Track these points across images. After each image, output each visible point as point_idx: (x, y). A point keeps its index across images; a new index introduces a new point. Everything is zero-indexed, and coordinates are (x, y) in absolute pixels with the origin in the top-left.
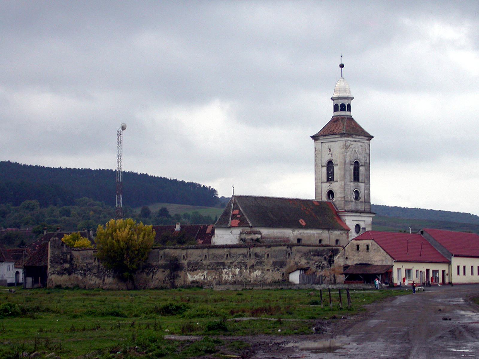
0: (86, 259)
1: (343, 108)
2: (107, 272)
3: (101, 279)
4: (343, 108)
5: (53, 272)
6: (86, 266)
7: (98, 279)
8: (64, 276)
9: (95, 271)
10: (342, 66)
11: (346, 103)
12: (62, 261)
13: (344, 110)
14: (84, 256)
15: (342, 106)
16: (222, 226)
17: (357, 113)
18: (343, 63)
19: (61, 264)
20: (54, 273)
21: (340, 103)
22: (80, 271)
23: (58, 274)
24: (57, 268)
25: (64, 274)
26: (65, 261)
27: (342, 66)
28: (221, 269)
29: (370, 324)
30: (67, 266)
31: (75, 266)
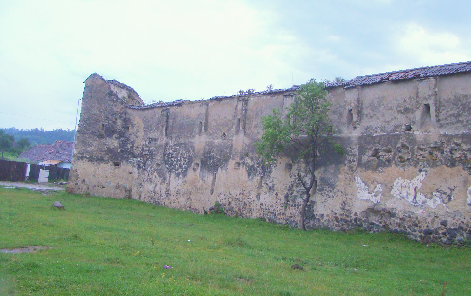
5: (82, 154)
8: (102, 165)
20: (82, 158)
23: (91, 160)
24: (90, 145)
26: (110, 132)
30: (113, 142)
31: (129, 146)
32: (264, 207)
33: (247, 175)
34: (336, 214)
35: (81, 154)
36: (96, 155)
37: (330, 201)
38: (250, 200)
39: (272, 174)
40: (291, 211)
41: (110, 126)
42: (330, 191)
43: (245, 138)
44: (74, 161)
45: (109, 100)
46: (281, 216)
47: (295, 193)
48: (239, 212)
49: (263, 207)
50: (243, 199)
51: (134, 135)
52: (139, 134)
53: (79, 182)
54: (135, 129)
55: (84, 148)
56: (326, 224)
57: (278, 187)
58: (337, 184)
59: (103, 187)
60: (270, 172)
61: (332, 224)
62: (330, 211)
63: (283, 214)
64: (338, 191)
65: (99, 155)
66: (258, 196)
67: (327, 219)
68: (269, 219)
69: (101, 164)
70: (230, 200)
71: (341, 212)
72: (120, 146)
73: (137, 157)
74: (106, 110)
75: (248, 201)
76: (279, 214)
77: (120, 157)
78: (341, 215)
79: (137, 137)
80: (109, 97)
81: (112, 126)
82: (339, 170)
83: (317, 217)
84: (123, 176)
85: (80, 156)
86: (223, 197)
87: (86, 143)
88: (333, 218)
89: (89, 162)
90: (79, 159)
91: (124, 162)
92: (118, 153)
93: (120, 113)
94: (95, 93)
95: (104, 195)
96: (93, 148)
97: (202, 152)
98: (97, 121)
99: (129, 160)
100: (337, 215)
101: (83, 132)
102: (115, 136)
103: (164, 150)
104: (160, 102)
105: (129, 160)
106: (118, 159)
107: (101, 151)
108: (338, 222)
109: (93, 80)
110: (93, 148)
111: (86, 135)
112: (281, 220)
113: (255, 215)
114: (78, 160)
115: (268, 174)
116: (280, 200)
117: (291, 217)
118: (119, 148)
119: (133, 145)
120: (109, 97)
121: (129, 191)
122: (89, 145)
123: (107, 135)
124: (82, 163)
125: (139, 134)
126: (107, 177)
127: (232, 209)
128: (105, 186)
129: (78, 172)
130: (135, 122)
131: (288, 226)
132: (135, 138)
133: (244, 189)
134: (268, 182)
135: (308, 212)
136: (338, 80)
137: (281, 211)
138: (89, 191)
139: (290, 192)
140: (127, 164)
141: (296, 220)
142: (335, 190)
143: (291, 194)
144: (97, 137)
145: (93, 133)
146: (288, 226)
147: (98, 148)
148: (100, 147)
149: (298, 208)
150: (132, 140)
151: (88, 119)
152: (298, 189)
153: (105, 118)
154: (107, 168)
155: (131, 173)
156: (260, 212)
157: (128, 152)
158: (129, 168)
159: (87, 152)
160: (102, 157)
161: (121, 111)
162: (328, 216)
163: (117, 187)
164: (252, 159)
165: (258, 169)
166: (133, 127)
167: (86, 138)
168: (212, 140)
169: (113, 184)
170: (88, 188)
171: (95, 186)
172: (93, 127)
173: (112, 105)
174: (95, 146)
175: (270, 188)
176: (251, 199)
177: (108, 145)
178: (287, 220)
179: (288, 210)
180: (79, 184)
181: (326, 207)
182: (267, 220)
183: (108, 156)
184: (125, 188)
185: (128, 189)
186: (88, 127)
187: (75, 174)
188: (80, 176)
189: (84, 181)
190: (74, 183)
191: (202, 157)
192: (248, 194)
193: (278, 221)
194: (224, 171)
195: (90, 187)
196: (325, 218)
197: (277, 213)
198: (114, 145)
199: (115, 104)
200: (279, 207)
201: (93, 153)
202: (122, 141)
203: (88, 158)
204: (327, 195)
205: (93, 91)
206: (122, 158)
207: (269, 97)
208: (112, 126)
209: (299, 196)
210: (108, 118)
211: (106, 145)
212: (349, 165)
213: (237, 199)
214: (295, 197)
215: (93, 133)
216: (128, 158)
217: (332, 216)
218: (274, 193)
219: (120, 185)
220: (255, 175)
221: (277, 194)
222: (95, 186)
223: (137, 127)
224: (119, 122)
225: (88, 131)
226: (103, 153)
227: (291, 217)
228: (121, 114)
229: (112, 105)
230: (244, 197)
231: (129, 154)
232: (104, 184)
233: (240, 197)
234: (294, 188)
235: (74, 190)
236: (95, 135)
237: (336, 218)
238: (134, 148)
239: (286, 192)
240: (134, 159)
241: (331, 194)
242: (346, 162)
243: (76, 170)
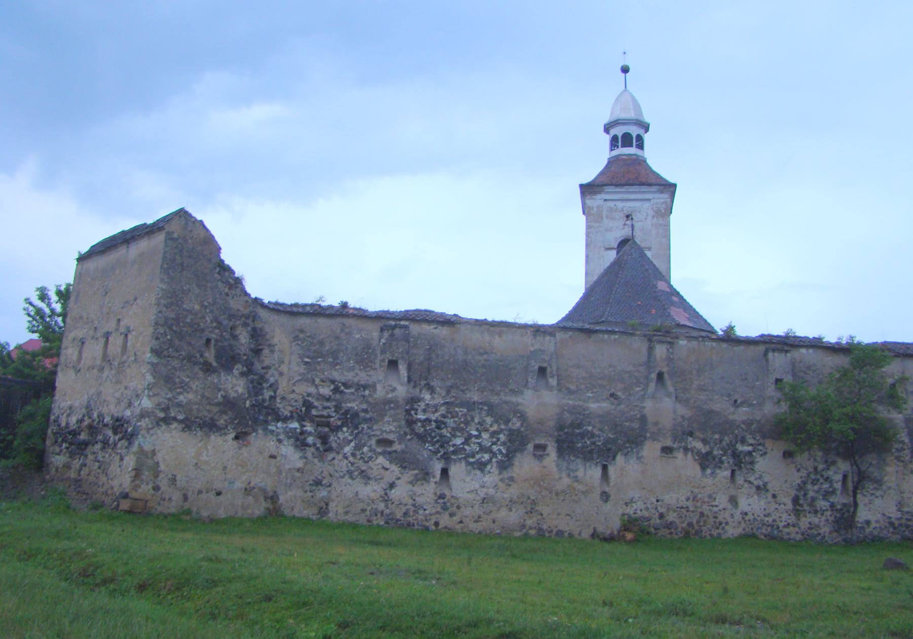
0: (334, 365)
1: (627, 140)
2: (467, 442)
3: (426, 475)
4: (627, 140)
5: (166, 409)
8: (215, 439)
9: (389, 427)
10: (625, 70)
11: (634, 131)
12: (210, 355)
13: (631, 146)
14: (322, 343)
15: (627, 135)
16: (528, 339)
17: (658, 157)
18: (627, 64)
19: (208, 368)
20: (167, 421)
21: (619, 131)
23: (188, 425)
24: (185, 387)
27: (625, 70)
28: (494, 455)
29: (137, 512)
30: (235, 385)
31: (267, 394)
33: (698, 468)
34: (890, 518)
35: (163, 410)
36: (200, 415)
37: (878, 502)
38: (715, 509)
39: (757, 467)
42: (874, 488)
43: (678, 406)
44: (148, 430)
45: (220, 280)
46: (791, 528)
47: (811, 494)
49: (750, 517)
50: (696, 507)
51: (276, 369)
53: (163, 483)
55: (170, 395)
56: (875, 533)
57: (774, 486)
59: (219, 494)
60: (752, 463)
61: (885, 532)
62: (879, 516)
63: (794, 526)
64: (889, 488)
65: (206, 414)
66: (733, 500)
67: (878, 525)
68: (765, 536)
69: (213, 437)
70: (661, 510)
71: (899, 515)
73: (285, 419)
74: (215, 303)
76: (785, 526)
78: (898, 519)
79: (281, 374)
80: (219, 273)
82: (884, 460)
84: (258, 464)
85: (162, 415)
86: (643, 506)
87: (175, 383)
89: (183, 430)
90: (159, 422)
91: (260, 431)
92: (247, 409)
93: (243, 315)
94: (190, 257)
96: (191, 396)
97: (552, 423)
98: (196, 330)
99: (270, 427)
100: (893, 520)
101: (165, 353)
102: (238, 368)
103: (408, 412)
104: (344, 305)
106: (247, 425)
107: (209, 404)
108: (895, 528)
109: (186, 224)
111: (175, 363)
112: (792, 536)
114: (158, 425)
115: (748, 466)
116: (785, 505)
117: (811, 528)
119: (275, 392)
120: (219, 273)
121: (272, 498)
122: (182, 387)
123: (223, 366)
124: (167, 435)
125: (284, 368)
126: (225, 468)
127: (669, 525)
129: (159, 457)
130: (275, 340)
131: (810, 541)
133: (696, 490)
134: (752, 479)
135: (845, 520)
137: (789, 521)
138: (187, 506)
139: (803, 493)
140: (266, 435)
141: (822, 531)
142: (884, 487)
143: (805, 495)
144: (201, 369)
146: (810, 541)
147: (203, 396)
149: (822, 515)
150: (272, 380)
151: (177, 320)
152: (816, 488)
153: (215, 325)
154: (222, 446)
157: (266, 408)
158: (271, 445)
159: (179, 405)
160: (212, 419)
162: (877, 522)
163: (248, 491)
164: (704, 441)
165: (724, 458)
166: (272, 352)
167: (175, 369)
169: (239, 485)
170: (186, 498)
171: (200, 492)
172: (189, 344)
174: (196, 392)
175: (758, 488)
176: (716, 506)
177: (225, 390)
179: (803, 519)
180: (163, 488)
181: (873, 511)
182: (762, 537)
183: (226, 418)
184: (264, 491)
185: (271, 494)
186: (177, 342)
188: (162, 467)
189: (173, 480)
190: (150, 486)
191: (556, 433)
193: (786, 537)
194: (633, 461)
195: (190, 494)
196: (873, 525)
197: (781, 524)
198: (236, 391)
199: (233, 292)
200: (785, 516)
201: (191, 410)
202: (252, 382)
203: (180, 422)
205: (185, 253)
206: (255, 421)
207: (724, 345)
210: (220, 323)
211: (220, 390)
213: (682, 508)
214: (813, 499)
215: (190, 358)
216: (266, 422)
217: (884, 521)
218: (769, 495)
219: (252, 485)
220: (720, 468)
221: (774, 496)
222: (200, 492)
223: (280, 351)
224: (244, 337)
225: (178, 351)
226: (215, 409)
227: (811, 528)
228: (247, 317)
229: (227, 295)
230: (699, 504)
231: (268, 414)
232: (218, 485)
233: (689, 504)
234: (809, 486)
235: (149, 505)
236: (195, 364)
237: (892, 524)
238: (278, 400)
239: (793, 493)
240: (279, 424)
241: (878, 493)
242: (894, 450)
243: (154, 452)
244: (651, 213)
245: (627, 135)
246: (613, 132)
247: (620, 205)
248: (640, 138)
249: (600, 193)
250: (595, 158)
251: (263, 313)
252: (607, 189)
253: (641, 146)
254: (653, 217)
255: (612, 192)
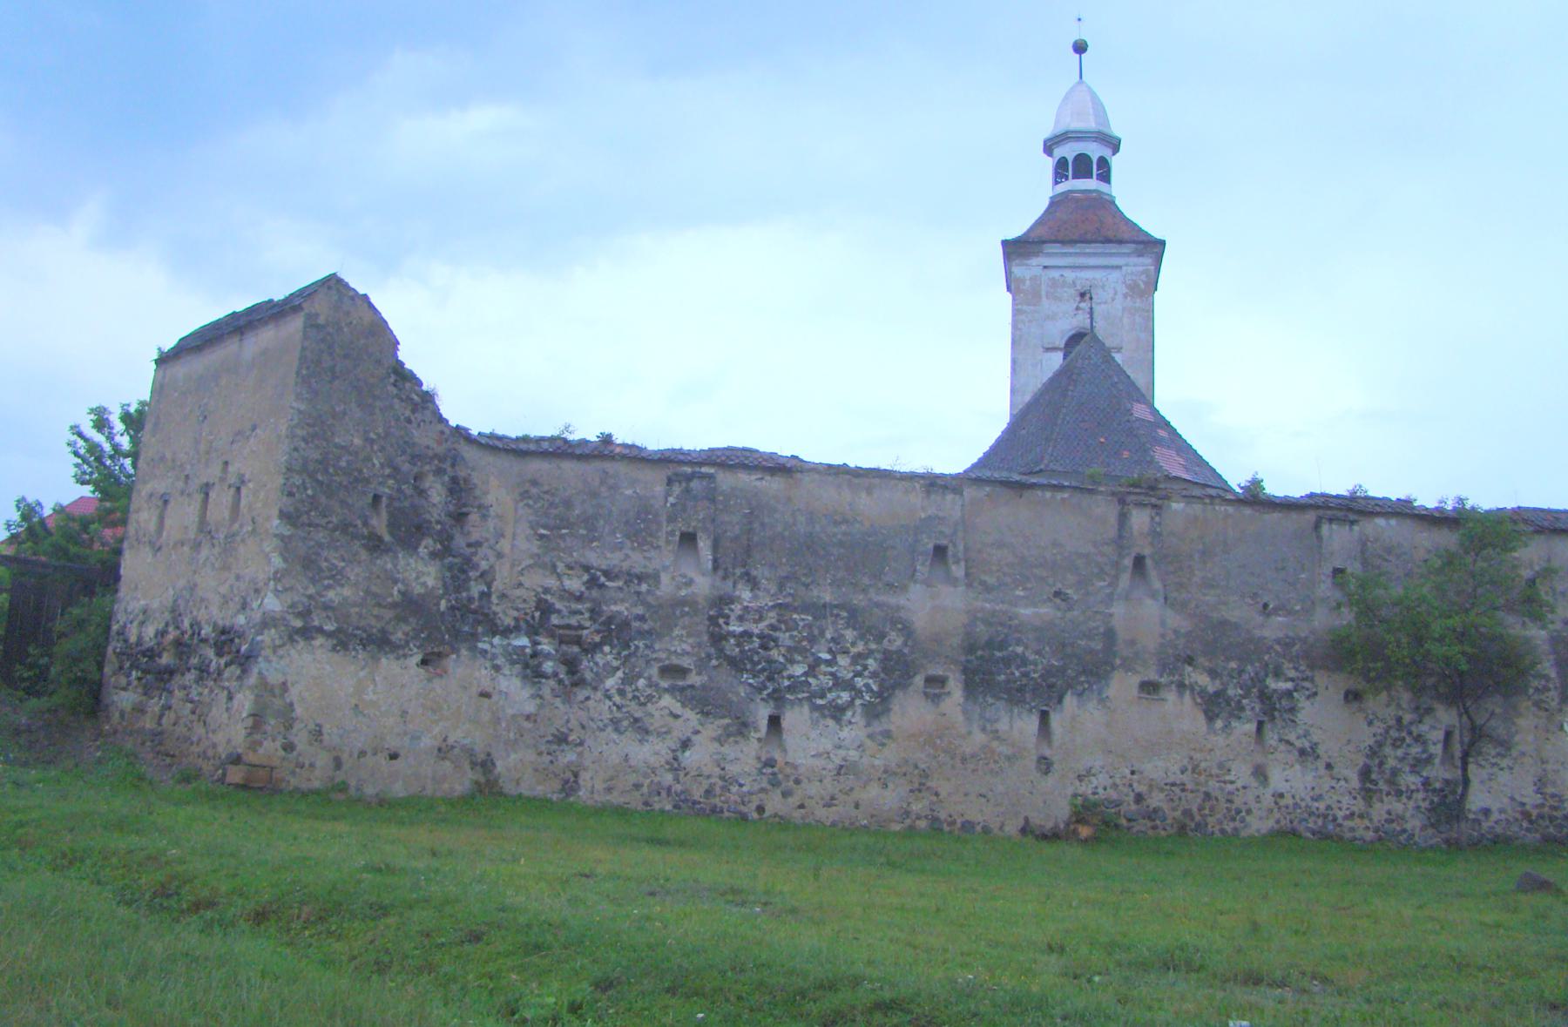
1: (1082, 166)
2: (812, 670)
3: (742, 727)
4: (1082, 166)
5: (305, 614)
6: (579, 598)
7: (713, 728)
8: (388, 664)
9: (680, 645)
10: (1080, 48)
11: (1094, 151)
14: (568, 503)
15: (1082, 159)
16: (916, 498)
17: (1135, 194)
19: (375, 545)
20: (307, 633)
21: (1069, 151)
22: (523, 641)
23: (342, 641)
24: (337, 577)
25: (394, 647)
26: (409, 530)
27: (1080, 48)
30: (421, 572)
31: (476, 589)
32: (1290, 802)
34: (1523, 804)
35: (300, 615)
36: (363, 623)
37: (1504, 777)
38: (1230, 787)
39: (1301, 717)
40: (1386, 807)
41: (406, 504)
43: (1169, 612)
44: (275, 649)
48: (1187, 821)
52: (505, 545)
53: (300, 738)
54: (491, 524)
55: (312, 591)
56: (1499, 830)
58: (1517, 738)
59: (394, 756)
62: (1506, 800)
63: (1361, 816)
64: (1523, 754)
65: (373, 622)
66: (1260, 773)
69: (384, 660)
71: (1538, 799)
72: (445, 586)
73: (506, 632)
74: (387, 434)
75: (1222, 789)
76: (1346, 818)
77: (448, 631)
79: (500, 555)
81: (413, 506)
83: (1471, 816)
85: (298, 623)
87: (321, 570)
88: (1518, 816)
89: (334, 649)
90: (293, 635)
91: (464, 652)
93: (436, 456)
94: (346, 356)
95: (398, 790)
96: (347, 592)
97: (956, 641)
98: (357, 480)
99: (480, 645)
101: (304, 518)
102: (427, 545)
103: (713, 620)
104: (607, 440)
105: (480, 645)
106: (442, 642)
107: (379, 605)
108: (1531, 822)
110: (347, 592)
111: (321, 536)
113: (1258, 825)
114: (292, 640)
115: (1286, 716)
116: (1346, 780)
118: (441, 598)
119: (489, 587)
121: (483, 764)
122: (333, 577)
124: (307, 657)
127: (1152, 814)
128: (402, 752)
129: (294, 694)
130: (490, 499)
131: (1389, 842)
132: (492, 559)
134: (1292, 737)
135: (1448, 805)
136: (1461, 500)
138: (340, 776)
141: (1408, 826)
142: (1514, 753)
143: (1381, 764)
145: (344, 527)
146: (1389, 842)
147: (368, 592)
148: (374, 589)
149: (1409, 798)
150: (484, 565)
151: (324, 462)
152: (1400, 752)
153: (387, 471)
155: (485, 695)
156: (1277, 815)
157: (475, 612)
158: (482, 675)
159: (327, 607)
160: (383, 631)
161: (440, 450)
162: (1501, 811)
163: (443, 751)
164: (1213, 673)
166: (484, 517)
167: (320, 545)
168: (1004, 607)
169: (427, 742)
170: (338, 763)
171: (363, 753)
173: (409, 421)
174: (356, 585)
175: (1302, 752)
176: (1232, 782)
177: (403, 582)
178: (1377, 830)
179: (1378, 805)
181: (1495, 792)
183: (407, 628)
184: (470, 752)
185: (482, 757)
186: (323, 500)
187: (278, 703)
189: (318, 733)
190: (278, 744)
192: (1215, 771)
195: (345, 757)
196: (1495, 816)
198: (424, 584)
199: (419, 416)
200: (1346, 800)
202: (450, 568)
203: (329, 635)
204: (1494, 765)
206: (456, 634)
207: (1248, 511)
208: (413, 506)
209: (1407, 769)
210: (396, 469)
211: (396, 582)
212: (1536, 697)
213: (1173, 784)
214: (1395, 772)
215: (344, 527)
216: (474, 637)
218: (1321, 765)
219: (451, 741)
221: (1329, 766)
222: (363, 753)
223: (498, 516)
224: (437, 493)
228: (442, 459)
230: (1202, 778)
232: (393, 743)
233: (1185, 778)
234: (1388, 750)
236: (355, 537)
237: (1526, 815)
238: (494, 599)
239: (1361, 761)
240: (497, 640)
241: (1504, 763)
242: (1531, 691)
244: (1122, 289)
245: (1082, 159)
246: (1059, 152)
247: (1070, 275)
248: (1104, 164)
249: (1036, 254)
250: (1029, 195)
251: (469, 453)
252: (1050, 248)
253: (1105, 177)
254: (1125, 296)
255: (1111, 255)
